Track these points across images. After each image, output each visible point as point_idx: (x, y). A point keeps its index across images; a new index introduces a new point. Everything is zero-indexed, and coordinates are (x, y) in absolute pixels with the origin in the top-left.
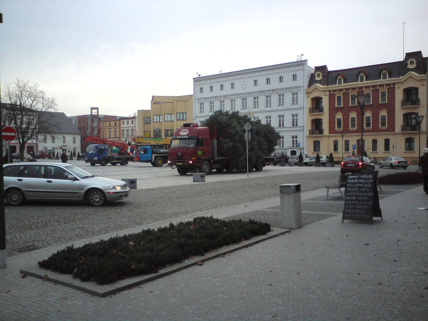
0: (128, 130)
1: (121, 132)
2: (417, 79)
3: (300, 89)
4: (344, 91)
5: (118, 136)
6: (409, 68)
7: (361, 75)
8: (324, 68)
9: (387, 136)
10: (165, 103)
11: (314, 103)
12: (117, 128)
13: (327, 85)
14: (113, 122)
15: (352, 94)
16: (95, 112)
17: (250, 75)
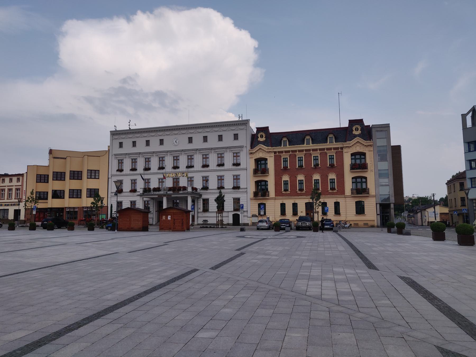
0: (10, 190)
2: (267, 151)
3: (242, 149)
4: (291, 153)
6: (354, 134)
8: (360, 122)
9: (295, 200)
13: (272, 147)
17: (200, 130)
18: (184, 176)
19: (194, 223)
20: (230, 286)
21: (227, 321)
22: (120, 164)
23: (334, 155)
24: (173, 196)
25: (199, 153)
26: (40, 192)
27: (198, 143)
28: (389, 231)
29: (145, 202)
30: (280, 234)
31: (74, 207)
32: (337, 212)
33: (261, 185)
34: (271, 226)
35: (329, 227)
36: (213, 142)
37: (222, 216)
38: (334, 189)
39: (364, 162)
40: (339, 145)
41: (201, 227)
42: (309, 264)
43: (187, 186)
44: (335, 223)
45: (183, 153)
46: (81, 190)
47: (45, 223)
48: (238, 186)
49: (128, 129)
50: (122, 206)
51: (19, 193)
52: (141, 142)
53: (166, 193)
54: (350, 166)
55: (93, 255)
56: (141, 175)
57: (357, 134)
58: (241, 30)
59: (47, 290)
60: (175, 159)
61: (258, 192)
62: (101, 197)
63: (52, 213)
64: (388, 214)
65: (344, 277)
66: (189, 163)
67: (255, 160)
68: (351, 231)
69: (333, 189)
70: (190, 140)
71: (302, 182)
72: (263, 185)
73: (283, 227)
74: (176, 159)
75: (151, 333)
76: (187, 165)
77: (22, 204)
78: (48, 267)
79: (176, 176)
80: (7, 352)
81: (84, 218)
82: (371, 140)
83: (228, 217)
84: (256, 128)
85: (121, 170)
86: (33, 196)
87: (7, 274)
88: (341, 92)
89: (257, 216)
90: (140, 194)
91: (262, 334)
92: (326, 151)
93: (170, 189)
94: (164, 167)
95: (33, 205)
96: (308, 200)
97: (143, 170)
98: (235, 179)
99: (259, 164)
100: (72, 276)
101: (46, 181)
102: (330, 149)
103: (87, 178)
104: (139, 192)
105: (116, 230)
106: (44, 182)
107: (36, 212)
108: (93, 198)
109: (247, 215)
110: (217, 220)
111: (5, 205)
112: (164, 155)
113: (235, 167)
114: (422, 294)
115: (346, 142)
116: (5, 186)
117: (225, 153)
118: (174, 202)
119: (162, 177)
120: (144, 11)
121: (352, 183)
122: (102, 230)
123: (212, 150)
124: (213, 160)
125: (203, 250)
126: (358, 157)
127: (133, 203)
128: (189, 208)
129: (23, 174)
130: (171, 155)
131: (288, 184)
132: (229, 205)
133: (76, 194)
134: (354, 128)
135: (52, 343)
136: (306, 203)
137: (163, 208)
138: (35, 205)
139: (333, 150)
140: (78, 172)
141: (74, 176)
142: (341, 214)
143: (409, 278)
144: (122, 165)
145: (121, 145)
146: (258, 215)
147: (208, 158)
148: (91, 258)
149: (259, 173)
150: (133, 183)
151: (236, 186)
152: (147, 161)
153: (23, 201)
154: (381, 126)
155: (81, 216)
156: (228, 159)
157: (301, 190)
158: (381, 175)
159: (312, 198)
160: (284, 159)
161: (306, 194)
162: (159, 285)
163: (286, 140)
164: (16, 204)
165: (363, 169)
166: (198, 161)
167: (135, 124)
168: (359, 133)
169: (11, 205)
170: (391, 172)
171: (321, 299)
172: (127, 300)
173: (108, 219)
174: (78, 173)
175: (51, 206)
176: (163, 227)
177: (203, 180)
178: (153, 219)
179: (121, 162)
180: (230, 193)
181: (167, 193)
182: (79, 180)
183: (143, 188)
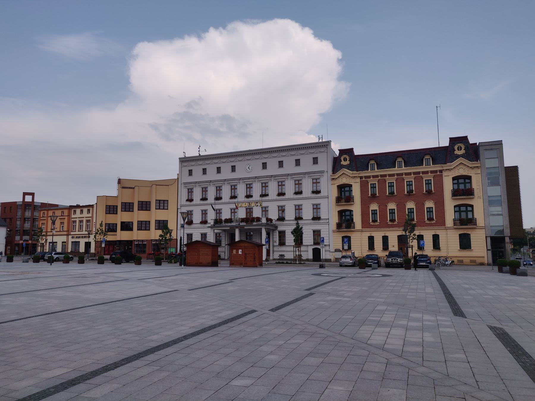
0: (81, 222)
2: (351, 176)
3: (323, 174)
4: (380, 178)
7: (427, 158)
8: (464, 139)
11: (339, 190)
12: (65, 218)
13: (357, 171)
14: (59, 210)
16: (28, 199)
18: (258, 206)
19: (270, 258)
20: (285, 330)
21: (269, 369)
22: (204, 193)
23: (431, 180)
24: (245, 228)
25: (275, 180)
26: (109, 224)
27: (273, 169)
28: (501, 271)
29: (216, 234)
30: (365, 272)
31: (143, 240)
32: (436, 246)
33: (345, 216)
34: (356, 263)
35: (424, 264)
36: (290, 167)
37: (300, 250)
38: (433, 219)
39: (470, 187)
40: (437, 167)
41: (276, 263)
42: (383, 308)
43: (261, 217)
44: (433, 260)
45: (256, 180)
46: (149, 221)
47: (114, 256)
48: (318, 216)
49: (198, 155)
50: (192, 239)
51: (90, 225)
52: (211, 169)
53: (238, 225)
54: (452, 192)
55: (152, 292)
57: (460, 154)
58: (321, 41)
59: (96, 328)
60: (263, 186)
61: (342, 224)
62: (170, 229)
63: (121, 246)
64: (503, 250)
65: (420, 324)
66: (263, 191)
67: (338, 186)
68: (452, 270)
69: (430, 219)
70: (264, 166)
71: (376, 212)
72: (348, 216)
73: (370, 263)
74: (249, 187)
75: (185, 378)
76: (261, 194)
77: (92, 237)
78: (104, 304)
79: (249, 206)
80: (41, 390)
81: (153, 252)
82: (479, 160)
83: (307, 251)
84: (339, 150)
85: (190, 200)
86: (102, 228)
87: (63, 310)
88: (440, 105)
89: (340, 251)
90: (210, 226)
91: (301, 385)
92: (421, 175)
93: (243, 220)
94: (236, 196)
95: (102, 237)
96: (400, 232)
97: (214, 199)
98: (315, 209)
99: (343, 191)
100: (125, 314)
101: (115, 212)
102: (427, 172)
103: (156, 209)
104: (210, 223)
105: (183, 265)
106: (113, 214)
107: (105, 245)
108: (161, 231)
109: (329, 250)
110: (295, 256)
111: (77, 237)
112: (267, 181)
113: (314, 195)
114: (510, 348)
115: (446, 163)
117: (209, 187)
118: (247, 234)
119: (234, 207)
120: (216, 27)
121: (455, 212)
122: (170, 265)
123: (256, 179)
124: (289, 188)
125: (270, 288)
126: (461, 181)
127: (204, 235)
128: (264, 242)
129: (93, 205)
130: (243, 183)
131: (377, 214)
132: (308, 238)
133: (144, 226)
134: (456, 147)
135: (86, 382)
136: (398, 236)
137: (236, 241)
138: (104, 238)
139: (430, 174)
140: (142, 202)
142: (441, 249)
143: (501, 329)
144: (206, 194)
145: (190, 173)
146: (342, 249)
147: (284, 185)
148: (149, 295)
149: (342, 201)
150: (204, 214)
151: (316, 216)
152: (218, 190)
153: (93, 233)
154: (491, 144)
155: (149, 250)
156: (307, 186)
157: (392, 220)
158: (491, 202)
159: (405, 230)
160: (372, 185)
161: (398, 226)
162: (209, 327)
163: (428, 158)
164: (87, 236)
165: (468, 195)
166: (273, 189)
167: (205, 150)
168: (462, 153)
169: (82, 237)
170: (504, 199)
171: (382, 349)
172: (171, 341)
173: (178, 253)
174: (142, 203)
175: (120, 239)
176: (235, 262)
177: (279, 210)
178: (225, 253)
179: (190, 191)
180: (310, 224)
181: (239, 224)
183: (214, 219)
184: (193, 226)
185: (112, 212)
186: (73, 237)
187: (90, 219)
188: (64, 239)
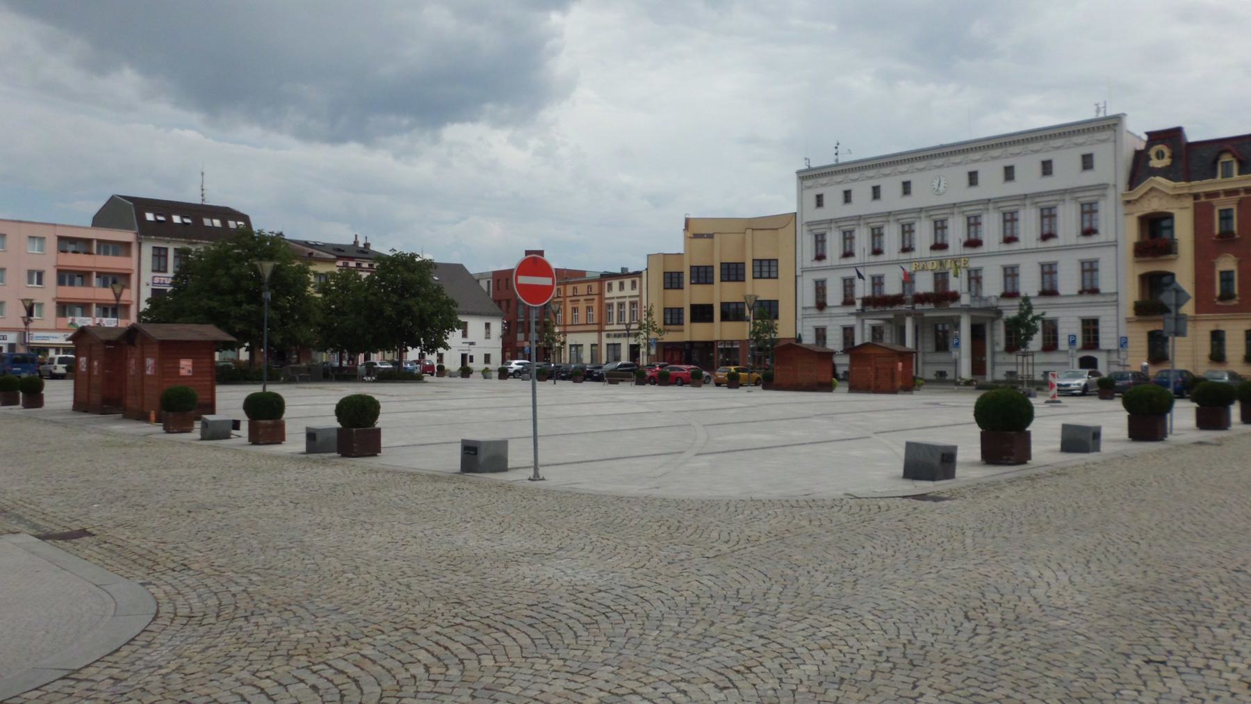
0: (621, 305)
1: (603, 308)
5: (596, 320)
10: (755, 232)
12: (593, 299)
13: (1188, 180)
15: (1221, 208)
38: (1232, 297)
56: (856, 267)
70: (973, 178)
111: (615, 336)
116: (625, 297)
133: (732, 313)
141: (729, 275)
145: (819, 200)
150: (1047, 273)
175: (691, 337)
179: (820, 240)
181: (913, 308)
182: (765, 278)
184: (827, 311)
185: (732, 277)
186: (608, 336)
187: (637, 299)
188: (592, 338)
